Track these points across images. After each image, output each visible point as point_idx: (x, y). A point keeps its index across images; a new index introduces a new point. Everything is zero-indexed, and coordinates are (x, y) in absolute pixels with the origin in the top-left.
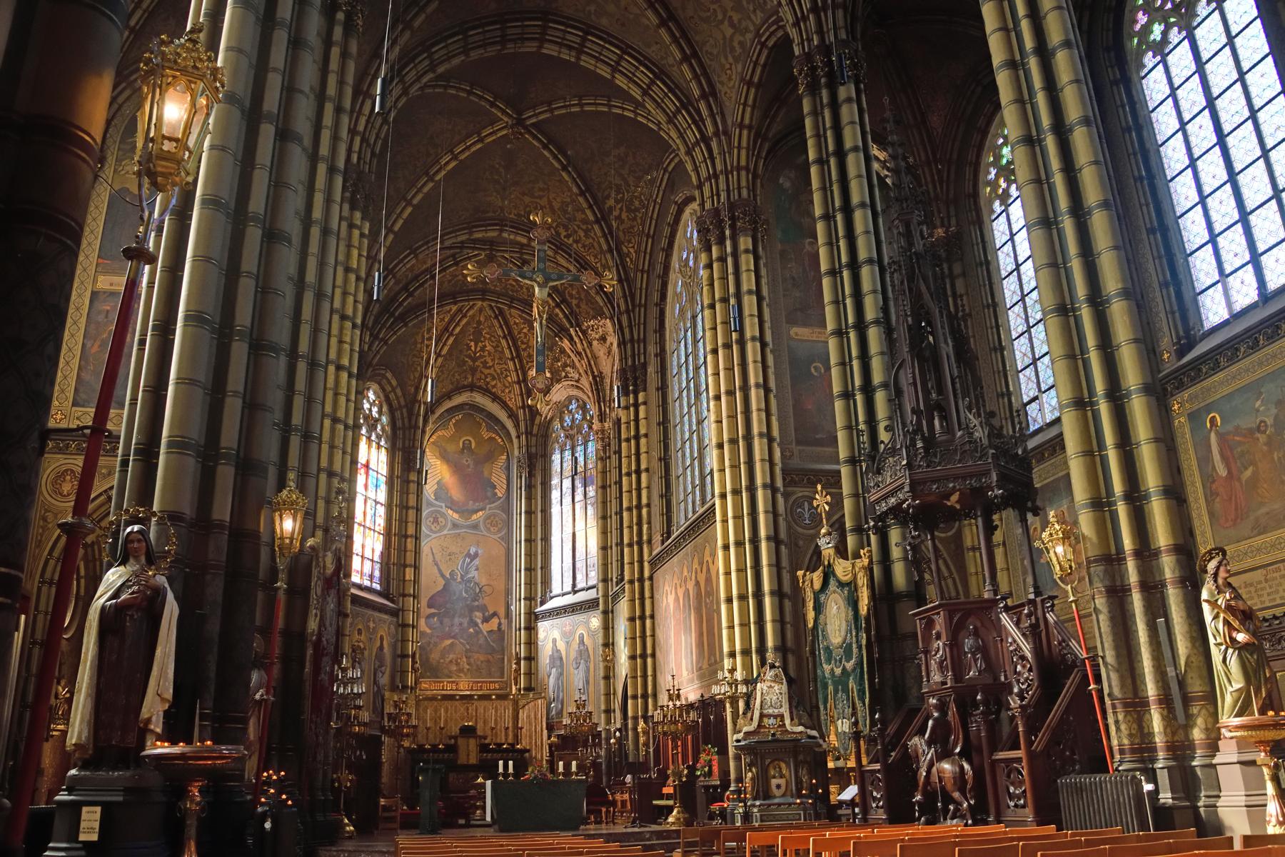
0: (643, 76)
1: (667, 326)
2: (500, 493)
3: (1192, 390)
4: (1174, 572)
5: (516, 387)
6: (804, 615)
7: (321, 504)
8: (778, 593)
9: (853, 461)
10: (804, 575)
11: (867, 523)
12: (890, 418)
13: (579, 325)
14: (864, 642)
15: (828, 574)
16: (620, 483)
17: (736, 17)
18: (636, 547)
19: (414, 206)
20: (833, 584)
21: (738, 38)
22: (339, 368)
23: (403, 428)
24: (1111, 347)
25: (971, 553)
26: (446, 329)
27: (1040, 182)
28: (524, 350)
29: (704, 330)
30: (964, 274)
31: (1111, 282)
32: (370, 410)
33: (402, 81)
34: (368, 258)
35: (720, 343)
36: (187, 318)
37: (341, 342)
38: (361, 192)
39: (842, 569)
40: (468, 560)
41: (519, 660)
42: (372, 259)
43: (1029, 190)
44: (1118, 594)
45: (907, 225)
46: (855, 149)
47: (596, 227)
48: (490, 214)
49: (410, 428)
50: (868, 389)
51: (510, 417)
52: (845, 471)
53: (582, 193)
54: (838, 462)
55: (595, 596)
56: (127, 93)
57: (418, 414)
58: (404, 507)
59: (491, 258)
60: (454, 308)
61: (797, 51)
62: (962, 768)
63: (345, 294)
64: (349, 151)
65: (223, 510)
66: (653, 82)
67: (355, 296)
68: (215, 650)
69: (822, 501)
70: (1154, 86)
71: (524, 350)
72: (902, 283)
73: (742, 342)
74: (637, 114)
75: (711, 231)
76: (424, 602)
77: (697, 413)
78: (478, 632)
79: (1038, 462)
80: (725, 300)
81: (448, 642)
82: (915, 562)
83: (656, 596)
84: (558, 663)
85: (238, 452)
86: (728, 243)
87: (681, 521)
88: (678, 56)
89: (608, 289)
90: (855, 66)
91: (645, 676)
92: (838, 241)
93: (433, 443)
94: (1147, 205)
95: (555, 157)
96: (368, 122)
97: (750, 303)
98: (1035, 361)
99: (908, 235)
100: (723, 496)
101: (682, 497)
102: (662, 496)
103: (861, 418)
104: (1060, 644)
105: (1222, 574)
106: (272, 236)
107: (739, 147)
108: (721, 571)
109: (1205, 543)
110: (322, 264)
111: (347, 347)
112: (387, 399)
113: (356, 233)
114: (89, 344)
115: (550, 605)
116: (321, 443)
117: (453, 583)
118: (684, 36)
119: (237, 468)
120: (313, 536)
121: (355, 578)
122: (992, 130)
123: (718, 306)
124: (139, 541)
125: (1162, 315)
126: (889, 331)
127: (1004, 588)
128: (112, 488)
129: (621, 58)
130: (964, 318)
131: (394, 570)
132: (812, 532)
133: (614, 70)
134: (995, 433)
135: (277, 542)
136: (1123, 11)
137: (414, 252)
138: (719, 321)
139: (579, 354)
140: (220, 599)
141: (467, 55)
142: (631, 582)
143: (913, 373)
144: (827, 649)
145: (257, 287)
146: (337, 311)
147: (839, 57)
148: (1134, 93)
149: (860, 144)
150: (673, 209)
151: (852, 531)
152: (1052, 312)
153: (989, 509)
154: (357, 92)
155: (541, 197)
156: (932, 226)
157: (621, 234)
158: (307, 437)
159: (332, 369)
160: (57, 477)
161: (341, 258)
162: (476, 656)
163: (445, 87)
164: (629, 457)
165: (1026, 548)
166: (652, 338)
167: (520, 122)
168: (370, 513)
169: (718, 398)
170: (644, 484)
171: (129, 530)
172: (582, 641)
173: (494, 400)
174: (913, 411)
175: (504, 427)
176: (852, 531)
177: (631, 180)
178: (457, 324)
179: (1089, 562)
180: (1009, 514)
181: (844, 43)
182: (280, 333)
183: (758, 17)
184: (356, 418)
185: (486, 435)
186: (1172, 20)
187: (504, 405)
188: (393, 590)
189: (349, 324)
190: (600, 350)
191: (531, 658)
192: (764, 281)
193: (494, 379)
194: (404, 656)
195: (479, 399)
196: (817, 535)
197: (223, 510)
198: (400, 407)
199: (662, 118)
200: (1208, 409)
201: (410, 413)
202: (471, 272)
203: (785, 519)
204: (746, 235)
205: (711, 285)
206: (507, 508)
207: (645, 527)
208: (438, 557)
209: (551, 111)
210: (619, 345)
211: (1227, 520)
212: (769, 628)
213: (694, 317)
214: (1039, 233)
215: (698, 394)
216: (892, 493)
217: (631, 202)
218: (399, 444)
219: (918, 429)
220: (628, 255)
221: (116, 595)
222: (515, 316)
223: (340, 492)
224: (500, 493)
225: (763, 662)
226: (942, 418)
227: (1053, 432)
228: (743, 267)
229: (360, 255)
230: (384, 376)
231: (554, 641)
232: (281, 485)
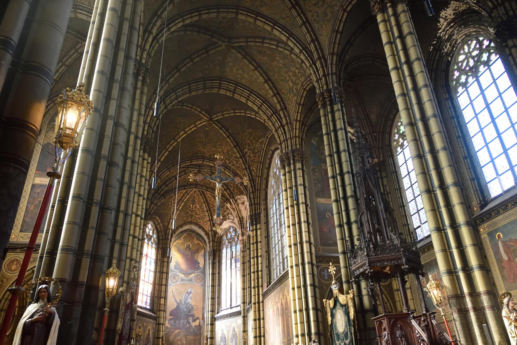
0: (259, 102)
1: (268, 198)
2: (201, 266)
3: (488, 223)
4: (488, 303)
5: (209, 222)
6: (327, 319)
7: (126, 272)
8: (315, 309)
9: (344, 253)
10: (326, 301)
11: (351, 279)
12: (359, 235)
13: (234, 198)
14: (353, 331)
15: (336, 301)
16: (250, 261)
17: (294, 79)
18: (256, 289)
19: (169, 151)
20: (338, 304)
21: (295, 87)
22: (137, 216)
23: (163, 240)
24: (451, 206)
25: (396, 292)
26: (181, 199)
27: (417, 140)
28: (212, 208)
29: (283, 200)
30: (386, 177)
31: (449, 179)
33: (165, 103)
34: (150, 171)
35: (289, 205)
36: (73, 197)
37: (138, 205)
38: (148, 146)
39: (342, 299)
40: (187, 295)
41: (207, 338)
42: (152, 172)
43: (412, 144)
44: (463, 312)
45: (363, 159)
46: (341, 129)
47: (240, 159)
48: (199, 155)
49: (165, 239)
50: (349, 223)
51: (206, 234)
52: (341, 257)
53: (235, 147)
54: (338, 253)
55: (239, 310)
56: (52, 105)
57: (169, 234)
58: (161, 273)
59: (199, 172)
60: (184, 191)
61: (318, 92)
63: (140, 186)
64: (143, 130)
65: (83, 277)
66: (262, 104)
67: (144, 187)
68: (75, 340)
69: (332, 270)
70: (462, 100)
71: (212, 208)
72: (361, 181)
73: (298, 205)
74: (256, 116)
75: (285, 161)
76: (168, 313)
77: (281, 233)
78: (190, 326)
79: (422, 253)
80: (291, 188)
81: (177, 331)
82: (373, 296)
83: (265, 310)
84: (224, 340)
85: (92, 252)
86: (292, 166)
87: (275, 277)
88: (272, 94)
89: (245, 184)
90: (340, 97)
91: (260, 328)
92: (335, 165)
93: (175, 246)
94: (463, 147)
95: (225, 133)
96: (151, 118)
97: (301, 189)
98: (418, 211)
99: (363, 162)
100: (292, 267)
101: (275, 267)
102: (267, 267)
103: (347, 235)
104: (439, 334)
105: (511, 305)
106: (111, 164)
107: (296, 129)
108: (292, 299)
109: (501, 290)
110: (131, 174)
111: (140, 207)
112: (156, 228)
113: (146, 162)
114: (29, 206)
115: (220, 314)
116: (128, 246)
117: (181, 305)
118: (274, 87)
119: (91, 259)
120: (122, 286)
122: (396, 120)
123: (288, 190)
124: (45, 292)
125: (472, 192)
126: (357, 200)
127: (412, 307)
128: (35, 267)
129: (250, 95)
130: (387, 193)
131: (156, 299)
132: (328, 282)
133: (247, 99)
134: (403, 242)
135: (106, 290)
136: (449, 71)
137: (169, 169)
138: (289, 196)
139: (234, 209)
140: (79, 317)
141: (190, 93)
142: (255, 304)
143: (367, 217)
144: (337, 334)
145: (104, 184)
146: (137, 193)
147: (334, 93)
148: (455, 103)
149: (343, 127)
150: (270, 152)
151: (345, 282)
152: (424, 192)
153: (403, 274)
154: (147, 107)
155: (219, 148)
156: (373, 158)
157: (250, 162)
158: (122, 244)
159: (134, 216)
160: (10, 263)
161: (139, 171)
162: (189, 337)
163: (182, 106)
164: (253, 251)
165: (420, 290)
166: (262, 203)
167: (211, 119)
168: (147, 275)
169: (289, 227)
170: (260, 262)
171: (41, 287)
172: (234, 330)
173: (199, 228)
174: (368, 233)
175: (203, 238)
176: (345, 282)
177: (254, 141)
178: (185, 198)
179: (449, 298)
180: (412, 276)
181: (336, 88)
182: (113, 202)
183: (302, 79)
184: (143, 236)
185: (196, 242)
186: (469, 74)
187: (204, 230)
188: (155, 308)
189: (141, 198)
190: (242, 207)
191: (212, 338)
192: (306, 180)
193: (200, 219)
194: (158, 338)
195: (194, 227)
196: (331, 284)
197: (83, 277)
198: (161, 231)
199: (266, 118)
200: (496, 231)
201: (165, 233)
202: (191, 177)
203: (317, 277)
204: (299, 163)
205: (286, 182)
206: (204, 272)
207: (260, 280)
208: (175, 294)
209: (223, 115)
210: (249, 206)
211: (510, 279)
212: (312, 324)
213: (279, 195)
214: (416, 161)
215: (281, 225)
216: (361, 267)
217: (254, 150)
218: (161, 246)
219: (371, 240)
220: (253, 170)
221: (32, 317)
222: (208, 194)
223: (135, 267)
224: (201, 266)
225: (310, 340)
226: (380, 235)
227: (427, 241)
228: (298, 175)
229: (147, 171)
230: (155, 218)
231: (222, 330)
232: (110, 265)
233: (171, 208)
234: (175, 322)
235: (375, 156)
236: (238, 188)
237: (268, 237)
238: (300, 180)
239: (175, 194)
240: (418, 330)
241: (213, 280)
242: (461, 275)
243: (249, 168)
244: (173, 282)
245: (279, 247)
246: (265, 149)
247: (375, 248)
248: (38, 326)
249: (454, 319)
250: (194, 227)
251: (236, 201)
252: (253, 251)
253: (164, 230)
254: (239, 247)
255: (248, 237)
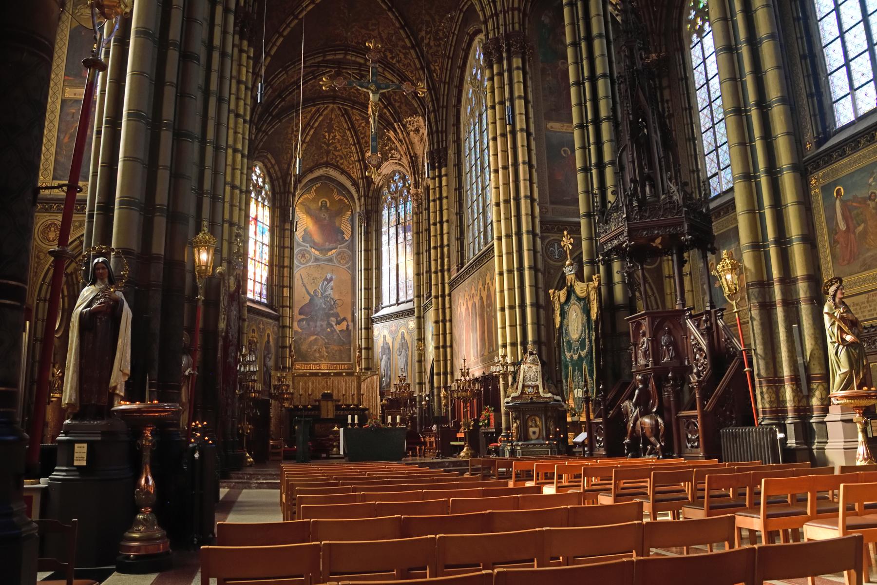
1: (462, 121)
2: (347, 237)
3: (824, 171)
5: (357, 164)
6: (554, 320)
8: (536, 305)
10: (554, 293)
11: (598, 257)
12: (615, 186)
13: (400, 121)
14: (593, 338)
15: (570, 292)
20: (573, 297)
22: (235, 151)
25: (668, 280)
26: (308, 124)
28: (363, 138)
29: (487, 124)
30: (669, 87)
31: (773, 92)
32: (257, 181)
34: (253, 73)
37: (236, 133)
39: (580, 288)
40: (326, 283)
42: (256, 75)
43: (718, 25)
44: (767, 307)
47: (412, 51)
48: (338, 42)
50: (600, 166)
51: (353, 185)
52: (583, 222)
58: (282, 247)
59: (338, 74)
62: (657, 421)
63: (238, 99)
65: (159, 247)
69: (567, 242)
71: (363, 138)
72: (626, 91)
73: (513, 133)
75: (492, 54)
76: (296, 311)
78: (334, 331)
79: (716, 218)
81: (313, 338)
82: (630, 284)
84: (387, 351)
86: (505, 63)
87: (471, 256)
89: (420, 95)
93: (301, 203)
98: (717, 148)
99: (631, 57)
100: (500, 239)
101: (471, 240)
102: (457, 239)
104: (726, 340)
105: (839, 295)
108: (498, 289)
109: (828, 272)
111: (240, 136)
112: (267, 172)
113: (244, 55)
116: (224, 203)
121: (250, 295)
123: (497, 107)
124: (103, 268)
127: (689, 303)
131: (276, 289)
132: (560, 264)
134: (687, 197)
135: (197, 269)
138: (498, 117)
139: (401, 141)
142: (436, 297)
144: (569, 342)
146: (233, 111)
150: (466, 38)
151: (587, 263)
153: (682, 248)
155: (373, 30)
156: (648, 52)
157: (430, 56)
161: (234, 73)
162: (332, 347)
164: (435, 212)
166: (451, 130)
168: (258, 251)
169: (496, 171)
171: (96, 261)
172: (403, 337)
174: (632, 181)
175: (349, 192)
176: (587, 263)
177: (437, 18)
178: (316, 121)
179: (748, 285)
184: (248, 186)
187: (349, 177)
188: (275, 303)
189: (241, 120)
190: (415, 139)
191: (369, 348)
192: (529, 90)
193: (342, 158)
194: (284, 347)
195: (333, 173)
196: (564, 265)
198: (278, 179)
201: (285, 183)
204: (518, 57)
205: (493, 92)
207: (446, 260)
210: (428, 135)
211: (844, 260)
213: (481, 115)
214: (723, 56)
215: (483, 169)
216: (616, 237)
217: (437, 33)
220: (435, 71)
221: (89, 305)
222: (356, 116)
223: (238, 235)
224: (347, 237)
225: (525, 351)
227: (728, 197)
229: (247, 72)
231: (385, 337)
232: (198, 230)
233: (291, 139)
234: (309, 325)
235: (652, 48)
236: (408, 104)
237: (459, 188)
238: (519, 89)
239: (298, 115)
240: (696, 334)
241: (367, 260)
242: (773, 250)
243: (428, 68)
244: (300, 263)
245: (478, 206)
246: (456, 32)
247: (641, 207)
248: (101, 319)
249: (751, 317)
250: (333, 173)
251: (404, 126)
252: (435, 212)
253: (282, 177)
254: (409, 205)
255: (425, 189)
